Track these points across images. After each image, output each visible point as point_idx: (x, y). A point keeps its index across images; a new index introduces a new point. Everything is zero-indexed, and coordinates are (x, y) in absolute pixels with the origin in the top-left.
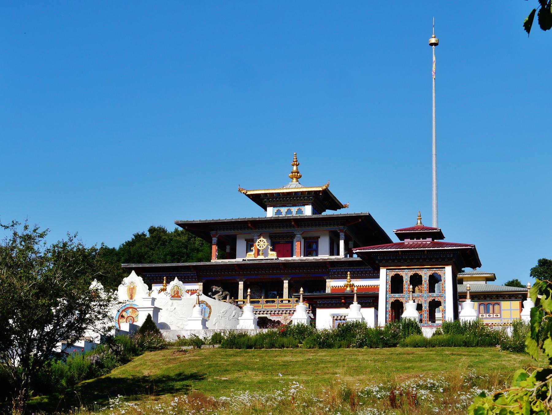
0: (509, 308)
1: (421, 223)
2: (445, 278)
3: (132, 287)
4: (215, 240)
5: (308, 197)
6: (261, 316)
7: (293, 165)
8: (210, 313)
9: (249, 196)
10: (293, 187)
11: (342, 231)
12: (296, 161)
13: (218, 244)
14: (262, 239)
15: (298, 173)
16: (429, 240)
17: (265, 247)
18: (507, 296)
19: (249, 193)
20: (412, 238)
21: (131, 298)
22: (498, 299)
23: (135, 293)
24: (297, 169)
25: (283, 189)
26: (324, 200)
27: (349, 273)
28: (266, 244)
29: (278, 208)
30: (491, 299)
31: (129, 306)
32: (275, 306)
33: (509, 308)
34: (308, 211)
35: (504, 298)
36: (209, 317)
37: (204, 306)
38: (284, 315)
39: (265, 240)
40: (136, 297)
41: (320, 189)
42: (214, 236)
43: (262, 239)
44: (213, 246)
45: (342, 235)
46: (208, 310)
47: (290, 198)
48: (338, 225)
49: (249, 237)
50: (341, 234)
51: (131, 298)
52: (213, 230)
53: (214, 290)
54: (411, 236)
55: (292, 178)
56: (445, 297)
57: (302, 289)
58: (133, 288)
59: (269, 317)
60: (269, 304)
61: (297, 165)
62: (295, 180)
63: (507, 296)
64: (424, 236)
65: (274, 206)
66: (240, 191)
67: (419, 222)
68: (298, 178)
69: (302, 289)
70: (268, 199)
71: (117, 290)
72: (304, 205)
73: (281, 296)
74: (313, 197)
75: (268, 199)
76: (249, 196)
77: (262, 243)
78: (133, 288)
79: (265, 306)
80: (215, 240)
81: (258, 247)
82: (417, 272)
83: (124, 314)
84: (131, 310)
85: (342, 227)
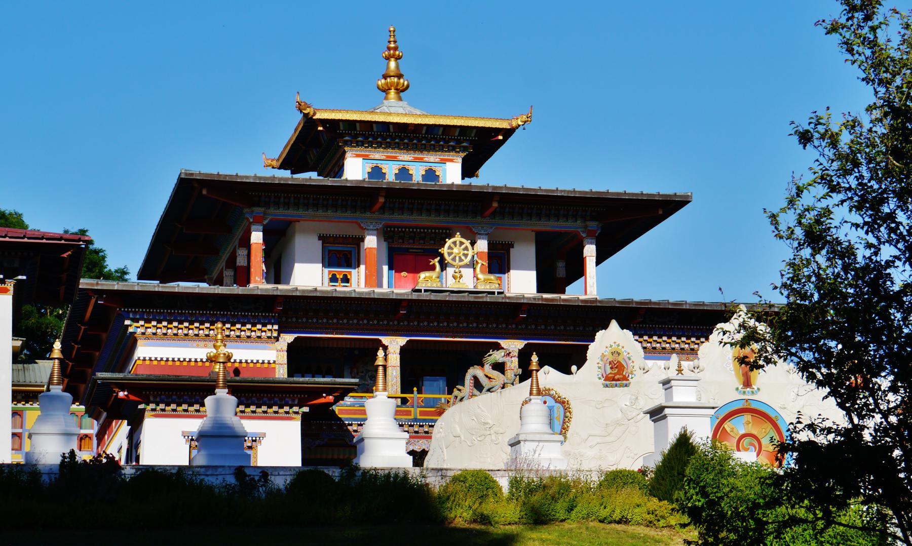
5: (458, 142)
7: (388, 58)
10: (395, 111)
11: (590, 234)
12: (396, 49)
14: (458, 238)
15: (400, 76)
24: (397, 67)
31: (739, 406)
34: (451, 173)
39: (449, 242)
49: (333, 229)
55: (385, 90)
61: (398, 58)
68: (400, 91)
74: (471, 142)
77: (456, 250)
85: (593, 225)
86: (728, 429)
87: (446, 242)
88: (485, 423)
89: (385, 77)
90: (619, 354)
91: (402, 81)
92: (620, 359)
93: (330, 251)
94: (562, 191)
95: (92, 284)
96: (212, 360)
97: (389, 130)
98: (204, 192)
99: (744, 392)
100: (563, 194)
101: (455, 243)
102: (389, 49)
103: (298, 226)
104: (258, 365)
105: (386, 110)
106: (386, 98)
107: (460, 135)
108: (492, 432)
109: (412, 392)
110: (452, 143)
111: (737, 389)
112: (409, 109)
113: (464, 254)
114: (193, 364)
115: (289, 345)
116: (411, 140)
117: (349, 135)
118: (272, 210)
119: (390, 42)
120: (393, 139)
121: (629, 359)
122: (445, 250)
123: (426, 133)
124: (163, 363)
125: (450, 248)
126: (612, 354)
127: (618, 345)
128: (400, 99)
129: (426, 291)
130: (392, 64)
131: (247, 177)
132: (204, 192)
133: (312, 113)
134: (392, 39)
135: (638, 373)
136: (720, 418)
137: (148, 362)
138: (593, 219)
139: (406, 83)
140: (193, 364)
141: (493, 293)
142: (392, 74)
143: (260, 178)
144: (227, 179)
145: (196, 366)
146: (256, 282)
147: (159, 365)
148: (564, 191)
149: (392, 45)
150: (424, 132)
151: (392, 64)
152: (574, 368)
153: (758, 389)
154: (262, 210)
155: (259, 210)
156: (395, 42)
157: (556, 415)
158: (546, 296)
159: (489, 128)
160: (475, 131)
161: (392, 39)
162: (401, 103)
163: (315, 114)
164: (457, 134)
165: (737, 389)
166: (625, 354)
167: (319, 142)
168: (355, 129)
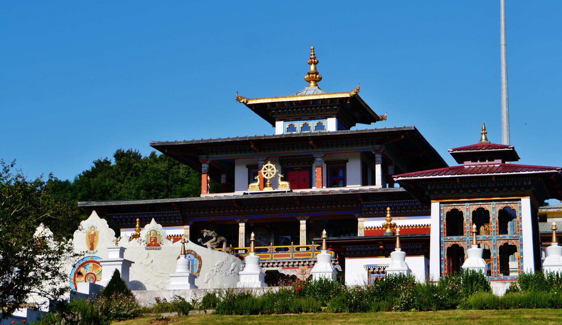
1: (486, 139)
2: (521, 214)
3: (92, 233)
4: (205, 167)
5: (332, 107)
6: (270, 269)
7: (310, 64)
8: (200, 267)
9: (250, 106)
10: (311, 93)
11: (378, 152)
12: (314, 58)
13: (209, 173)
14: (269, 164)
15: (317, 74)
16: (498, 162)
17: (273, 175)
19: (250, 102)
20: (483, 160)
21: (92, 249)
24: (315, 68)
26: (352, 110)
27: (388, 209)
28: (275, 171)
32: (289, 256)
34: (331, 125)
37: (192, 257)
38: (301, 267)
39: (273, 166)
40: (98, 247)
41: (348, 95)
42: (205, 163)
43: (269, 164)
45: (378, 157)
46: (197, 262)
47: (306, 108)
48: (372, 143)
49: (252, 162)
50: (377, 156)
51: (92, 249)
52: (203, 154)
54: (473, 157)
55: (309, 81)
56: (522, 240)
57: (324, 232)
58: (95, 234)
59: (280, 269)
60: (280, 253)
61: (315, 64)
62: (312, 84)
64: (491, 156)
65: (285, 120)
66: (238, 99)
67: (484, 137)
68: (316, 81)
69: (324, 232)
70: (277, 110)
71: (73, 238)
73: (297, 242)
74: (338, 106)
75: (277, 110)
76: (250, 106)
77: (269, 170)
78: (95, 234)
79: (275, 256)
80: (205, 167)
81: (264, 176)
82: (482, 206)
83: (82, 270)
84: (91, 265)
85: (377, 147)
87: (262, 167)
89: (309, 74)
95: (85, 204)
96: (386, 226)
97: (284, 106)
102: (311, 59)
104: (414, 227)
107: (330, 102)
109: (291, 245)
114: (377, 229)
115: (474, 212)
116: (302, 108)
117: (280, 109)
118: (210, 156)
125: (271, 167)
129: (250, 193)
130: (312, 67)
131: (181, 142)
133: (245, 102)
138: (377, 144)
140: (373, 229)
141: (285, 192)
146: (204, 193)
155: (203, 157)
156: (314, 55)
158: (299, 191)
163: (247, 102)
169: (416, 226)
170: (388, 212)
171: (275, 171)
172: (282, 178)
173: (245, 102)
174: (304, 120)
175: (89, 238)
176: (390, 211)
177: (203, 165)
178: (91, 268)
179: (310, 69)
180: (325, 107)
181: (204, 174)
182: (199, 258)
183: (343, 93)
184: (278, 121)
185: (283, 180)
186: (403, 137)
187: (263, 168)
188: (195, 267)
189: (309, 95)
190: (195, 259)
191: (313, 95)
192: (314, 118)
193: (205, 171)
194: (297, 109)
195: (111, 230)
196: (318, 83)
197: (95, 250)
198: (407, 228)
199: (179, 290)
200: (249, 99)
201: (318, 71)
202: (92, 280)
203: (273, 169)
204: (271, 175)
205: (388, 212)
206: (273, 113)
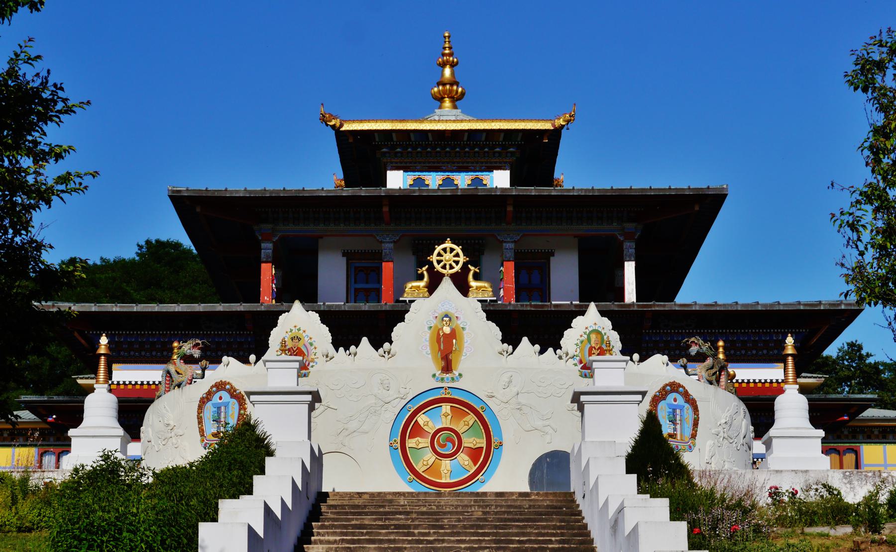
0: (883, 463)
3: (447, 330)
4: (267, 248)
5: (504, 147)
7: (443, 65)
8: (696, 424)
10: (447, 119)
11: (629, 236)
13: (275, 261)
14: (448, 245)
17: (457, 268)
18: (876, 432)
21: (447, 368)
22: (854, 437)
23: (460, 351)
24: (453, 74)
25: (422, 120)
27: (721, 343)
28: (462, 259)
29: (417, 174)
30: (839, 437)
31: (441, 394)
33: (883, 463)
35: (869, 437)
36: (694, 436)
37: (681, 400)
40: (463, 364)
42: (267, 239)
43: (448, 245)
44: (263, 265)
45: (629, 247)
49: (357, 244)
50: (627, 244)
51: (447, 368)
53: (694, 350)
55: (440, 99)
58: (453, 334)
61: (453, 65)
62: (447, 103)
63: (876, 432)
65: (406, 169)
66: (324, 120)
68: (456, 99)
71: (391, 342)
72: (490, 169)
75: (393, 147)
77: (448, 256)
78: (453, 334)
80: (267, 248)
81: (438, 267)
83: (421, 419)
84: (446, 408)
85: (630, 226)
86: (421, 422)
87: (435, 249)
88: (168, 425)
90: (299, 339)
91: (455, 87)
92: (300, 345)
93: (356, 268)
94: (579, 190)
97: (410, 139)
98: (198, 210)
99: (442, 379)
100: (580, 193)
101: (457, 255)
102: (444, 55)
103: (320, 241)
105: (437, 118)
106: (440, 107)
108: (173, 434)
110: (498, 150)
111: (434, 375)
112: (462, 117)
113: (450, 265)
116: (453, 148)
117: (386, 146)
119: (444, 48)
120: (434, 148)
121: (311, 344)
122: (434, 258)
123: (468, 140)
124: (138, 387)
125: (452, 250)
126: (292, 339)
127: (299, 330)
128: (455, 107)
131: (237, 191)
132: (198, 210)
133: (338, 125)
134: (447, 45)
135: (321, 360)
136: (412, 410)
137: (122, 387)
139: (460, 90)
142: (446, 81)
143: (251, 192)
144: (216, 194)
145: (141, 389)
147: (134, 389)
148: (582, 190)
149: (447, 51)
150: (465, 138)
151: (447, 72)
152: (252, 358)
153: (460, 375)
154: (270, 226)
156: (450, 48)
157: (230, 412)
159: (530, 130)
160: (520, 134)
161: (447, 45)
162: (455, 111)
163: (341, 126)
164: (501, 139)
165: (434, 375)
166: (306, 339)
167: (363, 155)
168: (392, 140)
169: (771, 382)
170: (721, 350)
171: (462, 259)
172: (475, 273)
173: (338, 125)
174: (444, 171)
175: (438, 341)
176: (724, 348)
177: (263, 245)
178: (446, 415)
179: (442, 75)
180: (492, 148)
181: (266, 262)
182: (693, 403)
183: (539, 120)
184: (392, 169)
185: (477, 277)
186: (697, 208)
187: (436, 252)
188: (686, 426)
189: (447, 121)
190: (687, 405)
191: (454, 121)
192: (465, 169)
193: (268, 256)
194: (434, 148)
195: (492, 326)
196: (457, 103)
197: (456, 373)
198: (752, 385)
199: (806, 471)
200: (345, 121)
201: (457, 80)
202: (450, 445)
203: (457, 255)
204: (451, 267)
205: (721, 350)
206: (385, 153)
